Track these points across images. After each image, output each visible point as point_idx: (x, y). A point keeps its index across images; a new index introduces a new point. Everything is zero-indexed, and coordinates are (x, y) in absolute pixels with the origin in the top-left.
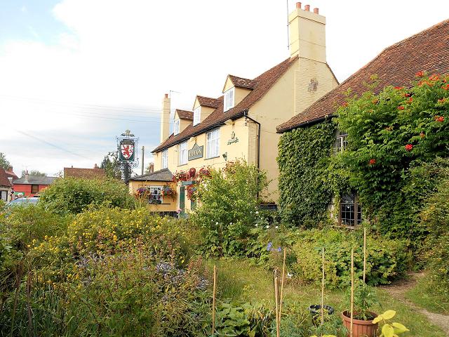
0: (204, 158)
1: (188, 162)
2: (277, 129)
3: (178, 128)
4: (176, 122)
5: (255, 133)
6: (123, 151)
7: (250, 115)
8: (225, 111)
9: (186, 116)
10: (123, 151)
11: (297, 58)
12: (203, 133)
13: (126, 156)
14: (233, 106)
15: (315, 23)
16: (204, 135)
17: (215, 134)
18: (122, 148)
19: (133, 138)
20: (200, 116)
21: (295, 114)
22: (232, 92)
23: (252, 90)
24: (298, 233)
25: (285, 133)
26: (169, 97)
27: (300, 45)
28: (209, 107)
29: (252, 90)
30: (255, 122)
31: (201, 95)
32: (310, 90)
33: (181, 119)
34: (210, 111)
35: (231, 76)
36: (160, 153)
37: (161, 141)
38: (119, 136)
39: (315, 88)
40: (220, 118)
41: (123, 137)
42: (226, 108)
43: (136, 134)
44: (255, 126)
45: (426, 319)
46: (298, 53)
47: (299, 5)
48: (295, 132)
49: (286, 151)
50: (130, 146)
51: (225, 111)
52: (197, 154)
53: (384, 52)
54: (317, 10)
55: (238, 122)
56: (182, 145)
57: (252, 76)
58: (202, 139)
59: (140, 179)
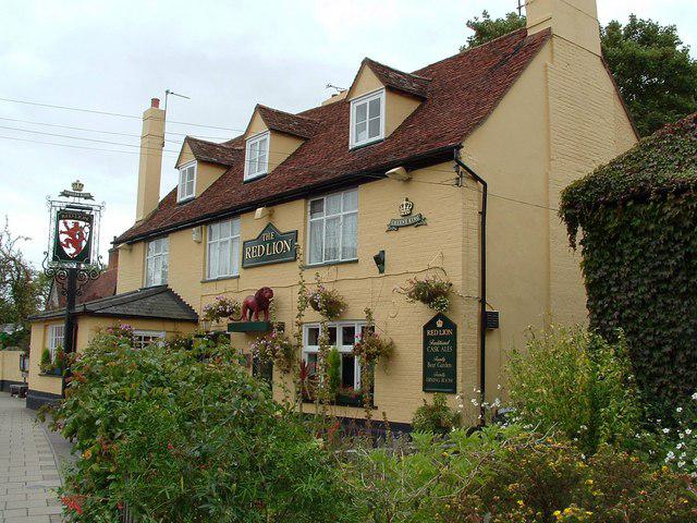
5: (477, 207)
6: (63, 237)
8: (247, 177)
17: (339, 206)
18: (62, 228)
19: (89, 202)
20: (261, 160)
22: (191, 170)
26: (161, 106)
33: (202, 162)
34: (214, 175)
36: (139, 248)
38: (55, 197)
40: (237, 197)
41: (64, 199)
42: (358, 138)
44: (473, 192)
45: (90, 352)
50: (82, 224)
52: (273, 250)
56: (216, 227)
58: (291, 217)
59: (119, 310)
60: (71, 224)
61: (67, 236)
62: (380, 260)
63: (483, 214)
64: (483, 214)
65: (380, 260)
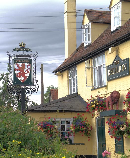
18: (16, 67)
50: (26, 64)
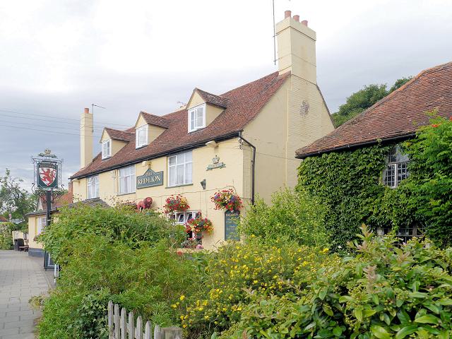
0: (165, 186)
1: (135, 190)
2: (297, 154)
3: (109, 149)
4: (105, 143)
5: (251, 158)
7: (244, 135)
8: (190, 130)
9: (124, 138)
10: (42, 176)
11: (289, 75)
12: (164, 156)
13: (47, 182)
14: (204, 126)
15: (308, 39)
16: (164, 159)
18: (41, 171)
20: (144, 137)
21: (319, 137)
23: (225, 108)
24: (335, 275)
25: (308, 159)
26: (90, 112)
27: (293, 60)
28: (157, 126)
29: (225, 108)
30: (250, 145)
31: (145, 112)
32: (301, 114)
34: (120, 146)
35: (143, 113)
37: (82, 165)
39: (306, 111)
43: (59, 155)
46: (290, 69)
47: (288, 13)
48: (329, 158)
49: (312, 178)
50: (51, 169)
51: (190, 130)
52: (152, 180)
53: (423, 74)
54: (305, 23)
55: (223, 145)
57: (161, 113)
58: (159, 165)
60: (45, 169)
61: (44, 175)
62: (203, 184)
63: (253, 162)
64: (253, 162)
65: (203, 184)
